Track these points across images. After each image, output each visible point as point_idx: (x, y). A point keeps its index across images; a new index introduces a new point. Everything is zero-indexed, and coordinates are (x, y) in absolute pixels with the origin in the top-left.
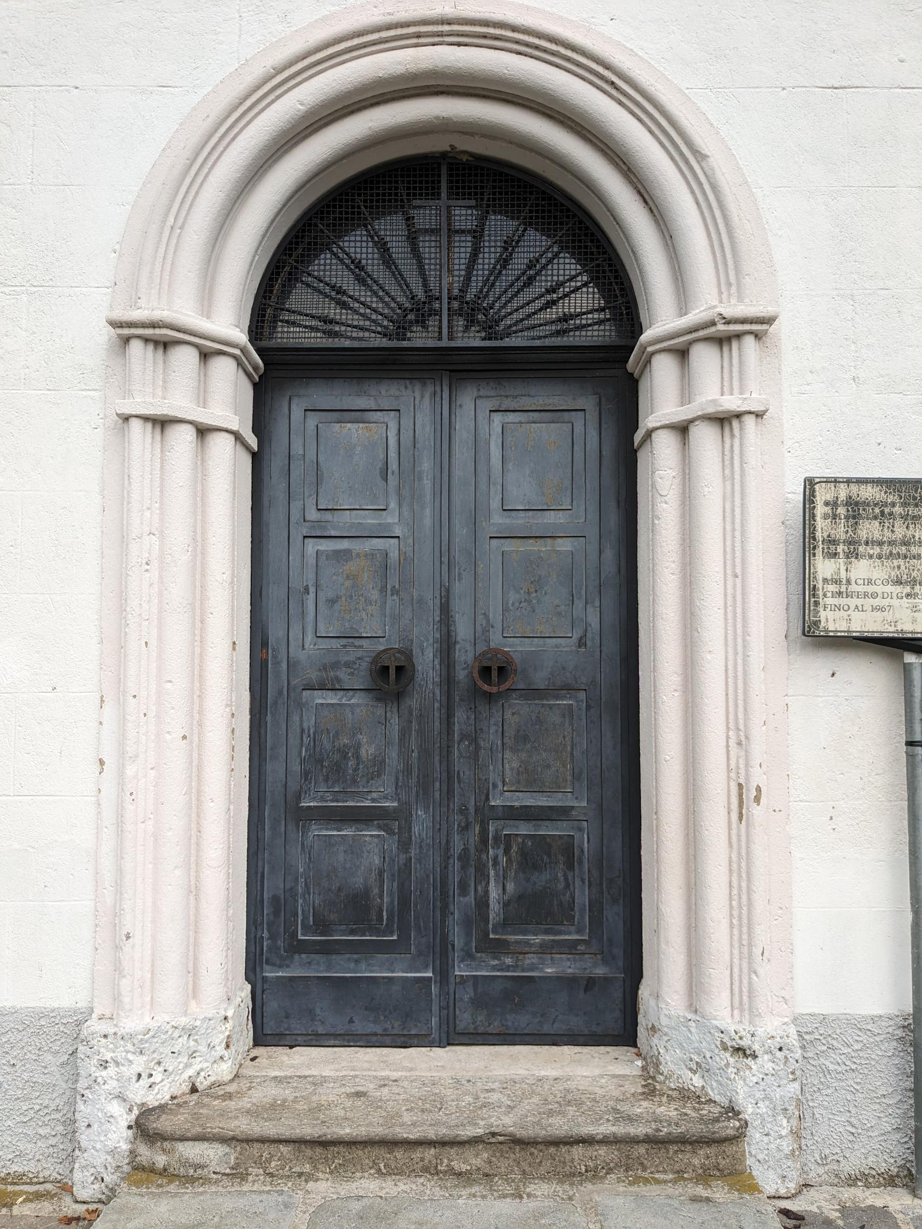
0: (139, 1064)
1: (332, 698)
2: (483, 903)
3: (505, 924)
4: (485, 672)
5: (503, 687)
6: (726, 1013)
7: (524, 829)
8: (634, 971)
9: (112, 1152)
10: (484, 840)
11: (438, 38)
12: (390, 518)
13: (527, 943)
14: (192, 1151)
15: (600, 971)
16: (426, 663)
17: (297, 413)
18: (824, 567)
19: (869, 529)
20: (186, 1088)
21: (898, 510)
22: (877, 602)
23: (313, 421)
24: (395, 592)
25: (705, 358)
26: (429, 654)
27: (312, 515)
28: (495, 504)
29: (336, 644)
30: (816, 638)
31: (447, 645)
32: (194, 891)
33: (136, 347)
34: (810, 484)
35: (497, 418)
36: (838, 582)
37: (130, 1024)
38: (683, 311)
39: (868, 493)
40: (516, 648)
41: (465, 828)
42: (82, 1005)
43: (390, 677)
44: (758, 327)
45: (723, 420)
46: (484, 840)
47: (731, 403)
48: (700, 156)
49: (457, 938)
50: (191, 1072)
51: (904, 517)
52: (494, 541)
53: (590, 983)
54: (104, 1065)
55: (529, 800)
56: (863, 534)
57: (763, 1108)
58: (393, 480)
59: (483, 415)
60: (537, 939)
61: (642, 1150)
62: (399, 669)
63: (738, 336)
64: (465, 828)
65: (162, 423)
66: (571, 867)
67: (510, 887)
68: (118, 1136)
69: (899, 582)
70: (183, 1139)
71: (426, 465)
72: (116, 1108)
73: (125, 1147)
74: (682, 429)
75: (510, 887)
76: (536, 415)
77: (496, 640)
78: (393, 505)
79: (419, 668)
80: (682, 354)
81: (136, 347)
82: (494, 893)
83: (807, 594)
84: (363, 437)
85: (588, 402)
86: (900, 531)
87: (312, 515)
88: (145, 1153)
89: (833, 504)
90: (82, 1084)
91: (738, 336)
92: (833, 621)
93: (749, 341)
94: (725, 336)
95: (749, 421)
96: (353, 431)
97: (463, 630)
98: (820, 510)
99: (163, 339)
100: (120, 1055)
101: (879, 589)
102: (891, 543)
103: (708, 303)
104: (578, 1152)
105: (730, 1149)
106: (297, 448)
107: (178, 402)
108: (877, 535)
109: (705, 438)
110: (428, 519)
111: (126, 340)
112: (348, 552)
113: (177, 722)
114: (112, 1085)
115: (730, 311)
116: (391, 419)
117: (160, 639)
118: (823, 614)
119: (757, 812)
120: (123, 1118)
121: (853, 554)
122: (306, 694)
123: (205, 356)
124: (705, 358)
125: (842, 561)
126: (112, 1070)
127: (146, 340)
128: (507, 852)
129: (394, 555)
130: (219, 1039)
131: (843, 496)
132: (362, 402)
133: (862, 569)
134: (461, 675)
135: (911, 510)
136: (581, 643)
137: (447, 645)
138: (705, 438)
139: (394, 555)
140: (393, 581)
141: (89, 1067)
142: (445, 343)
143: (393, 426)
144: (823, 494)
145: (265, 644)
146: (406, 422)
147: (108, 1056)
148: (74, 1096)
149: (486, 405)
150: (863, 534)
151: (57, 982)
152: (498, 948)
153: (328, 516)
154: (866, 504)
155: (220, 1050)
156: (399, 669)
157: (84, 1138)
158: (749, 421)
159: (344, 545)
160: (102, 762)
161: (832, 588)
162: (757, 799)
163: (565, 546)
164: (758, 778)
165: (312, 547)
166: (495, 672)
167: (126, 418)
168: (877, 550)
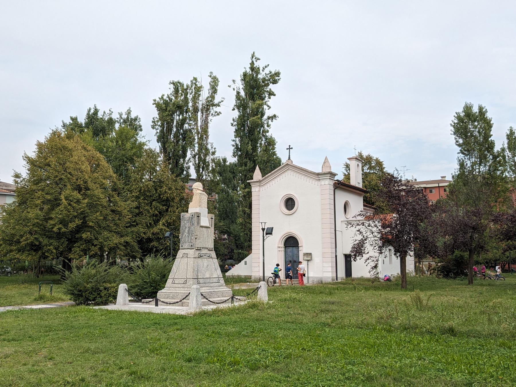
43: (291, 261)
84: (290, 249)
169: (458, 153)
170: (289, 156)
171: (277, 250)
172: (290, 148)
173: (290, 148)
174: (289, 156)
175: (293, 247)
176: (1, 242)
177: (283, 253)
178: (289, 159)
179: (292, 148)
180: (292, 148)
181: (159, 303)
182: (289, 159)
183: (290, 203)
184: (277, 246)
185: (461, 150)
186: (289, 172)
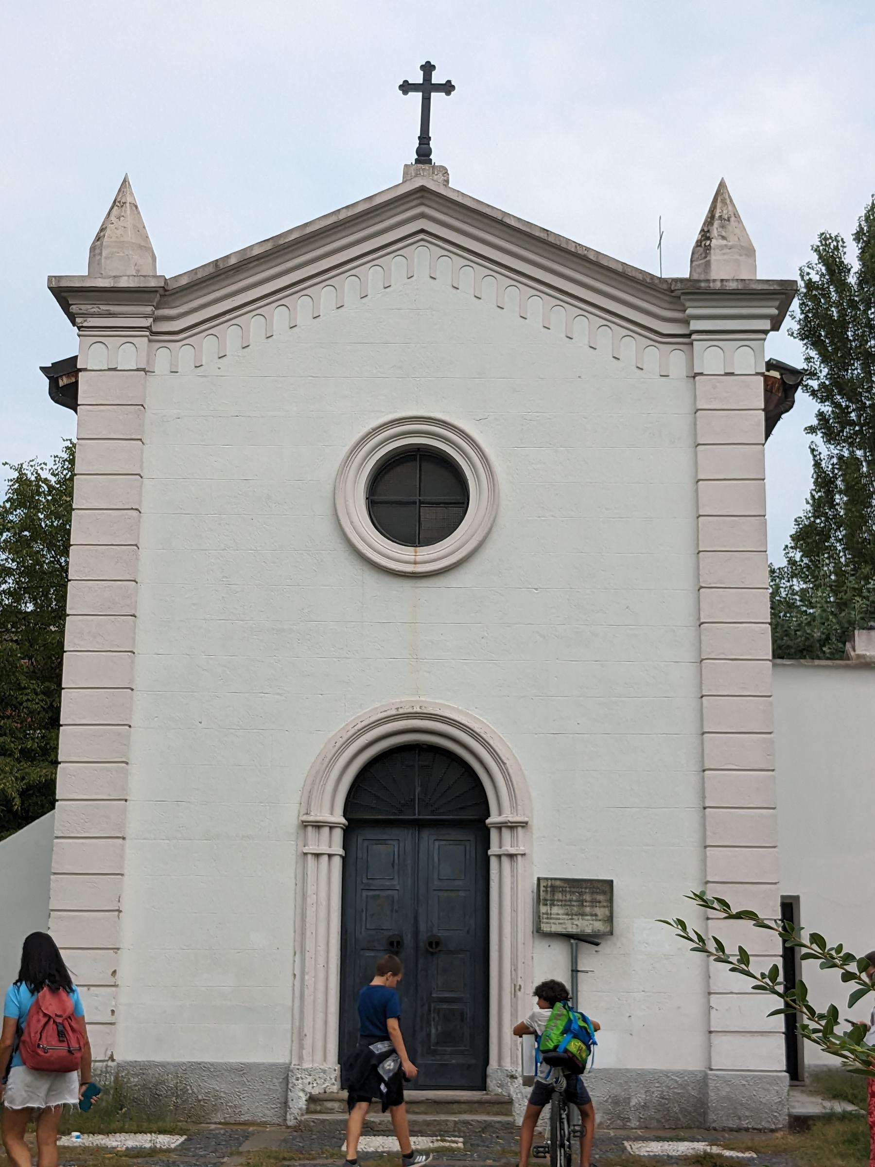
0: (310, 1079)
1: (372, 954)
2: (429, 1035)
3: (437, 1044)
4: (430, 944)
5: (438, 949)
6: (509, 1065)
7: (445, 1006)
8: (486, 1062)
9: (300, 1109)
10: (430, 1010)
11: (415, 718)
12: (395, 882)
13: (445, 1051)
14: (329, 1105)
15: (473, 1061)
16: (408, 940)
17: (360, 841)
18: (543, 909)
19: (558, 896)
20: (322, 1091)
21: (568, 889)
22: (561, 921)
23: (366, 843)
24: (396, 912)
25: (506, 833)
26: (409, 936)
27: (365, 881)
28: (436, 876)
29: (373, 932)
30: (539, 933)
31: (416, 933)
32: (326, 1022)
33: (310, 829)
34: (539, 879)
35: (437, 843)
36: (547, 914)
37: (307, 1065)
38: (500, 815)
39: (558, 883)
40: (442, 934)
41: (422, 1006)
42: (287, 1061)
43: (395, 945)
44: (524, 825)
45: (511, 856)
46: (430, 1010)
47: (512, 851)
48: (504, 764)
49: (419, 1050)
50: (325, 1086)
51: (570, 892)
52: (436, 892)
53: (469, 1067)
54: (297, 1079)
55: (447, 995)
56: (556, 898)
57: (519, 1096)
58: (396, 867)
59: (431, 841)
60: (449, 1049)
61: (476, 1105)
62: (398, 943)
63: (517, 827)
64: (422, 1006)
65: (317, 855)
66: (462, 1020)
67: (439, 1028)
68: (302, 1103)
69: (567, 914)
70: (326, 1100)
71: (409, 862)
72: (302, 1094)
73: (304, 1107)
74: (499, 856)
75: (439, 1028)
76: (451, 842)
77: (435, 931)
78: (396, 877)
79: (405, 942)
80: (500, 829)
81: (310, 829)
82: (433, 1031)
83: (538, 919)
84: (386, 848)
85: (472, 838)
86: (568, 897)
87: (365, 881)
88: (312, 1106)
89: (546, 887)
90: (290, 1086)
91: (517, 827)
92: (545, 928)
93: (520, 829)
94: (512, 827)
95: (519, 857)
96: (381, 848)
97: (422, 927)
98: (542, 889)
99: (318, 826)
100: (303, 1076)
101: (561, 917)
102: (565, 901)
103: (508, 816)
104: (455, 1106)
105: (506, 1106)
106: (360, 855)
107: (324, 848)
108: (561, 898)
109: (505, 861)
110: (409, 881)
111: (306, 826)
112: (378, 896)
113: (321, 961)
114: (300, 1086)
115: (511, 819)
116: (395, 843)
117: (316, 931)
118: (542, 925)
119: (519, 994)
120: (304, 1098)
121: (552, 905)
122: (362, 952)
123: (331, 828)
124: (506, 833)
125: (549, 907)
126: (300, 1081)
127: (313, 826)
128: (438, 1015)
129: (396, 897)
130: (333, 1076)
131: (549, 884)
132: (385, 837)
133: (555, 910)
134: (422, 945)
135: (573, 890)
136: (468, 932)
137: (416, 933)
138: (505, 861)
139: (396, 897)
140: (396, 908)
141: (292, 1080)
142: (416, 817)
143: (396, 846)
144: (543, 884)
145: (346, 932)
146: (402, 845)
147: (299, 1076)
148: (287, 1090)
149: (433, 838)
150: (556, 898)
151: (277, 1054)
152: (434, 1053)
153: (371, 881)
154: (557, 887)
155: (333, 1081)
156: (398, 943)
157: (291, 1104)
158: (519, 857)
159: (377, 893)
160: (295, 975)
161: (545, 916)
162: (520, 990)
163: (462, 894)
164: (520, 982)
165: (365, 893)
166: (434, 944)
167: (306, 854)
168: (560, 903)
169: (811, 430)
170: (424, 138)
171: (287, 850)
172: (427, 86)
173: (427, 86)
174: (424, 138)
175: (419, 825)
176: (872, 316)
177: (327, 884)
178: (424, 154)
179: (448, 88)
180: (448, 88)
181: (772, 913)
182: (424, 154)
183: (418, 490)
184: (291, 818)
185: (821, 415)
186: (422, 255)
